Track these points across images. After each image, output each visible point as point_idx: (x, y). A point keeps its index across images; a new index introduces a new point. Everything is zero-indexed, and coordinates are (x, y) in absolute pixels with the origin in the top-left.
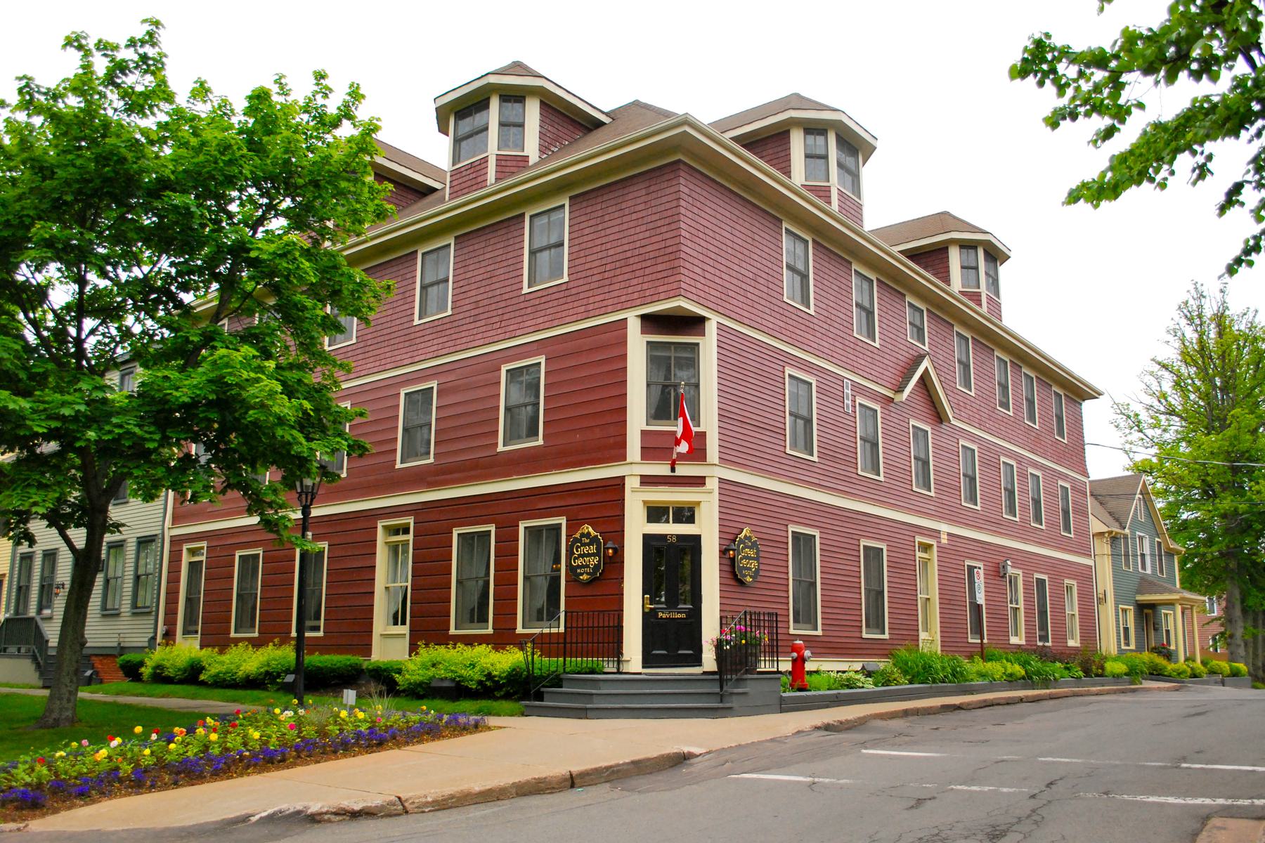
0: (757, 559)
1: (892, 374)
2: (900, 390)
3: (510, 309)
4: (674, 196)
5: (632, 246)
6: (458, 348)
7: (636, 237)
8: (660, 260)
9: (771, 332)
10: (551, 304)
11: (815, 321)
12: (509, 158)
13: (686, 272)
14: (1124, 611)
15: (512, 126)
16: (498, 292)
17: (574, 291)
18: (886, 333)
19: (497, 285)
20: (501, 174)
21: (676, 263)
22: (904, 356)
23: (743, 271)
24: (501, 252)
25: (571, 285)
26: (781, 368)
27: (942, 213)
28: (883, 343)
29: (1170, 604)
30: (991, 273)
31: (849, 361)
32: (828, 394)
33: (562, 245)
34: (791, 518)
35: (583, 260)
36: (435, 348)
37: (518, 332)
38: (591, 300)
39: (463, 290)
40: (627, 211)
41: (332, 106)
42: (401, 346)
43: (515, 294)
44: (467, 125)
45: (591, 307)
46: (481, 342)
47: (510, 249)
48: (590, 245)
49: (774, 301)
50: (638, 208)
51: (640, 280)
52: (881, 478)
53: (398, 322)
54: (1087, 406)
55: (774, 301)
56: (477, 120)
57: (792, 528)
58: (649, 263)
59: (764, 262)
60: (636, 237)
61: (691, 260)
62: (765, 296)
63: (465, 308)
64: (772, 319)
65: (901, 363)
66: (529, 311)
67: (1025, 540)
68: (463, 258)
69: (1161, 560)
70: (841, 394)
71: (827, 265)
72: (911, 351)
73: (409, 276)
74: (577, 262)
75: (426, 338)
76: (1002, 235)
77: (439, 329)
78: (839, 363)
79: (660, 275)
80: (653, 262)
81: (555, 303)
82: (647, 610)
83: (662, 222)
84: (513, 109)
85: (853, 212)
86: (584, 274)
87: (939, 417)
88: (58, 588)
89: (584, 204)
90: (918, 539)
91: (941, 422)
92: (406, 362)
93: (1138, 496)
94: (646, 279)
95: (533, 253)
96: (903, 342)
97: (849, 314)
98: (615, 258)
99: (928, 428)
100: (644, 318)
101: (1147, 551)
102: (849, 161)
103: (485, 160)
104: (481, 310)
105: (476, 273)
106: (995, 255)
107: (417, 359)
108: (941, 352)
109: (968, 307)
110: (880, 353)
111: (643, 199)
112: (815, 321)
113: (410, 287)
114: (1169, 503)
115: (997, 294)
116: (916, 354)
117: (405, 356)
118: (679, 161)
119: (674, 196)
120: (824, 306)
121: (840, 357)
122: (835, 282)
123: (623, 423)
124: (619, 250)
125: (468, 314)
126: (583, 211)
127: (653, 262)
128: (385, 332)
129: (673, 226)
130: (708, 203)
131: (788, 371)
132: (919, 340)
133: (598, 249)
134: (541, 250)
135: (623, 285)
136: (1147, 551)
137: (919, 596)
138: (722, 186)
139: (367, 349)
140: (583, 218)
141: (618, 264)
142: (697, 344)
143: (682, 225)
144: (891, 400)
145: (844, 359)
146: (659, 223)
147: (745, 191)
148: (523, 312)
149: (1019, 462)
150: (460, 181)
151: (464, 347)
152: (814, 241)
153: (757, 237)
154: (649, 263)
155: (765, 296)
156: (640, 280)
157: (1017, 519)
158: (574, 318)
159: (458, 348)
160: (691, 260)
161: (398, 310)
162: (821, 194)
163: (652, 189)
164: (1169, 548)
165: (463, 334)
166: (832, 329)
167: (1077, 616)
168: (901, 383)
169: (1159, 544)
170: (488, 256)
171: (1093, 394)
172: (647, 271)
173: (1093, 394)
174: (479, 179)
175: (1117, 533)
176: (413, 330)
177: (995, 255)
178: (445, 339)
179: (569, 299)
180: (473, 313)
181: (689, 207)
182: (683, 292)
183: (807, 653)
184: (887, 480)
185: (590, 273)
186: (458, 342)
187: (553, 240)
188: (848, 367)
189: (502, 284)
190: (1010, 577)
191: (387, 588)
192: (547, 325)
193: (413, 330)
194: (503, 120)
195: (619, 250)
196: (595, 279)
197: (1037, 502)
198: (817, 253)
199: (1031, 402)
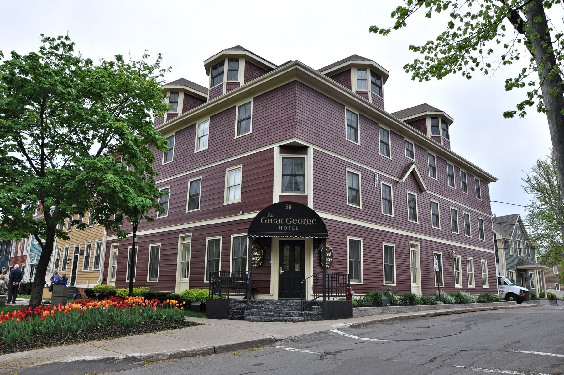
0: (331, 257)
1: (399, 171)
2: (401, 178)
3: (230, 145)
4: (293, 95)
5: (277, 117)
6: (210, 162)
7: (278, 113)
8: (287, 123)
9: (339, 153)
10: (245, 143)
11: (361, 148)
12: (232, 84)
13: (298, 127)
14: (512, 273)
15: (233, 71)
16: (225, 139)
17: (254, 137)
18: (395, 153)
19: (225, 136)
20: (228, 90)
21: (294, 123)
22: (404, 164)
23: (326, 127)
24: (227, 122)
25: (253, 134)
26: (344, 168)
27: (424, 104)
28: (393, 157)
29: (532, 269)
30: (445, 129)
31: (377, 165)
32: (367, 179)
33: (250, 118)
34: (348, 233)
35: (258, 124)
36: (201, 162)
37: (232, 155)
38: (261, 140)
39: (213, 138)
40: (275, 103)
41: (150, 62)
42: (190, 162)
43: (232, 139)
44: (216, 72)
45: (260, 143)
46: (218, 159)
47: (230, 120)
48: (260, 117)
49: (341, 139)
50: (279, 101)
51: (280, 131)
52: (393, 216)
53: (189, 152)
54: (491, 185)
55: (341, 139)
56: (220, 69)
57: (349, 238)
58: (283, 124)
59: (336, 123)
60: (278, 113)
61: (300, 122)
62: (336, 137)
63: (213, 146)
64: (340, 147)
65: (402, 167)
66: (237, 146)
67: (463, 242)
68: (213, 125)
69: (528, 252)
70: (373, 180)
71: (367, 125)
72: (407, 161)
73: (193, 133)
74: (256, 125)
75: (199, 159)
76: (449, 112)
77: (203, 154)
78: (372, 166)
79: (288, 129)
80: (285, 123)
81: (247, 142)
82: (281, 273)
83: (289, 106)
84: (233, 64)
85: (379, 102)
86: (258, 130)
87: (420, 189)
88: (68, 261)
89: (259, 101)
90: (410, 242)
91: (422, 192)
92: (190, 169)
93: (516, 223)
94: (282, 131)
95: (239, 122)
96: (403, 157)
97: (377, 145)
98: (270, 122)
99: (416, 194)
100: (281, 147)
101: (522, 247)
102: (378, 82)
103: (222, 85)
104: (219, 146)
105: (217, 131)
106: (447, 121)
107: (195, 167)
108: (421, 162)
109: (434, 143)
110: (392, 162)
111: (281, 97)
112: (361, 148)
113: (193, 138)
114: (67, 126)
115: (448, 137)
116: (409, 163)
117: (190, 166)
118: (296, 81)
119: (293, 95)
120: (365, 142)
121: (373, 164)
122: (370, 132)
123: (272, 192)
124: (271, 119)
125: (214, 148)
126: (258, 104)
127: (285, 123)
128: (184, 156)
129: (293, 108)
130: (309, 98)
131: (347, 169)
132: (411, 157)
133: (264, 119)
134: (243, 121)
135: (273, 133)
136: (522, 247)
137: (411, 267)
138: (366, 117)
139: (177, 164)
140: (259, 106)
141: (271, 125)
142: (304, 158)
143: (297, 107)
144: (398, 182)
145: (375, 164)
146: (287, 107)
147: (328, 94)
148: (235, 146)
149: (459, 209)
150: (213, 94)
151: (212, 162)
152: (360, 114)
153: (332, 113)
154: (283, 124)
155: (336, 137)
156: (280, 131)
157: (458, 233)
158: (254, 148)
159: (210, 162)
160: (300, 122)
161: (189, 147)
162: (364, 95)
163: (285, 93)
164: (531, 245)
165: (212, 156)
166: (369, 152)
167: (487, 275)
168: (402, 175)
169: (527, 244)
170: (222, 124)
171: (494, 180)
172: (283, 127)
173: (494, 180)
174: (220, 93)
175: (507, 239)
176: (194, 155)
177: (447, 121)
178: (205, 159)
179: (252, 140)
180: (216, 147)
181: (300, 99)
182: (296, 136)
183: (353, 293)
184: (396, 217)
185: (260, 129)
186: (210, 160)
187: (247, 116)
188: (377, 168)
189: (227, 135)
190: (455, 258)
191: (182, 263)
192: (243, 151)
193: (194, 155)
194: (230, 68)
195: (271, 119)
196: (262, 131)
197: (468, 226)
198: (361, 119)
199: (464, 183)
